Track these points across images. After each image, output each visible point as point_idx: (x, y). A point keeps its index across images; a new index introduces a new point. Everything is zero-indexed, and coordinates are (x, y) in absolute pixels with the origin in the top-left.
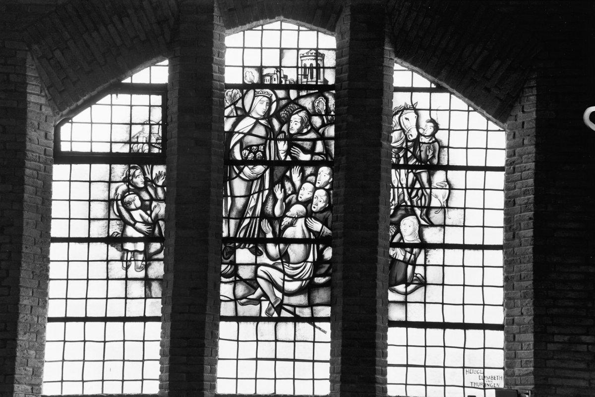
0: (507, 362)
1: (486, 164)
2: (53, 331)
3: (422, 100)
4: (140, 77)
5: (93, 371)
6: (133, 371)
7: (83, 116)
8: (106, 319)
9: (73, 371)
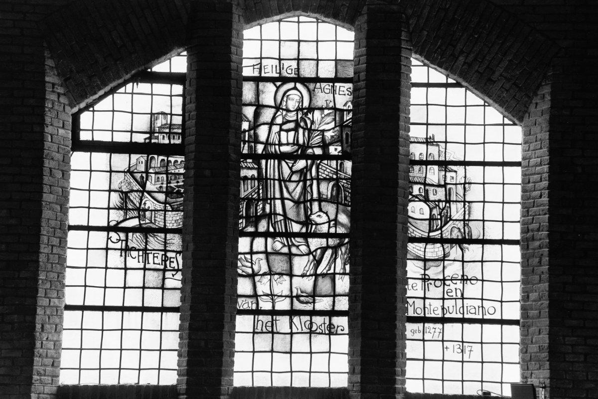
0: (523, 288)
1: (502, 317)
2: (70, 319)
3: (437, 95)
4: (161, 67)
5: (110, 359)
6: (150, 360)
7: (105, 104)
8: (123, 309)
9: (90, 359)
